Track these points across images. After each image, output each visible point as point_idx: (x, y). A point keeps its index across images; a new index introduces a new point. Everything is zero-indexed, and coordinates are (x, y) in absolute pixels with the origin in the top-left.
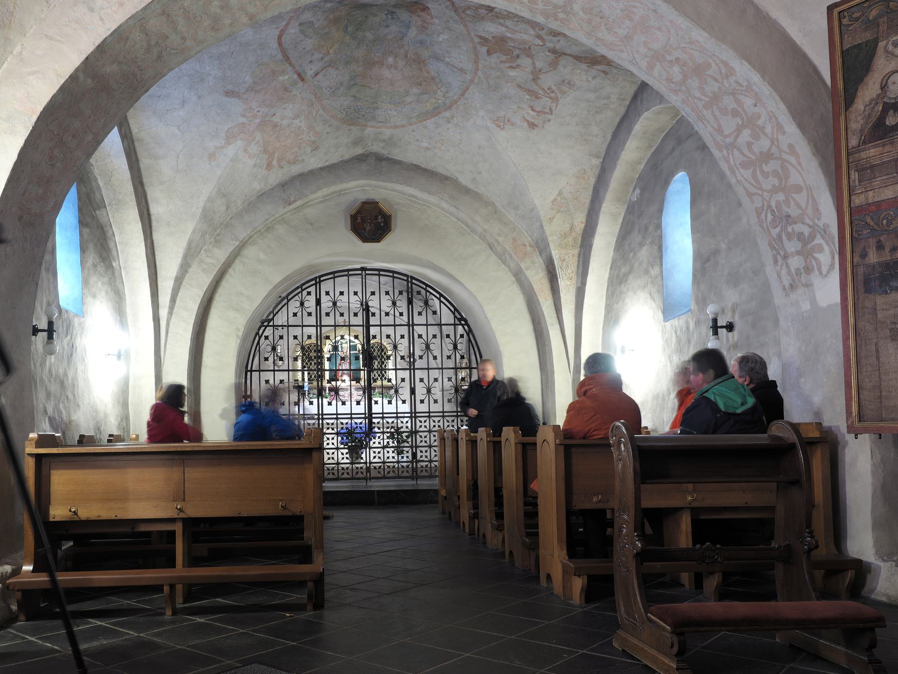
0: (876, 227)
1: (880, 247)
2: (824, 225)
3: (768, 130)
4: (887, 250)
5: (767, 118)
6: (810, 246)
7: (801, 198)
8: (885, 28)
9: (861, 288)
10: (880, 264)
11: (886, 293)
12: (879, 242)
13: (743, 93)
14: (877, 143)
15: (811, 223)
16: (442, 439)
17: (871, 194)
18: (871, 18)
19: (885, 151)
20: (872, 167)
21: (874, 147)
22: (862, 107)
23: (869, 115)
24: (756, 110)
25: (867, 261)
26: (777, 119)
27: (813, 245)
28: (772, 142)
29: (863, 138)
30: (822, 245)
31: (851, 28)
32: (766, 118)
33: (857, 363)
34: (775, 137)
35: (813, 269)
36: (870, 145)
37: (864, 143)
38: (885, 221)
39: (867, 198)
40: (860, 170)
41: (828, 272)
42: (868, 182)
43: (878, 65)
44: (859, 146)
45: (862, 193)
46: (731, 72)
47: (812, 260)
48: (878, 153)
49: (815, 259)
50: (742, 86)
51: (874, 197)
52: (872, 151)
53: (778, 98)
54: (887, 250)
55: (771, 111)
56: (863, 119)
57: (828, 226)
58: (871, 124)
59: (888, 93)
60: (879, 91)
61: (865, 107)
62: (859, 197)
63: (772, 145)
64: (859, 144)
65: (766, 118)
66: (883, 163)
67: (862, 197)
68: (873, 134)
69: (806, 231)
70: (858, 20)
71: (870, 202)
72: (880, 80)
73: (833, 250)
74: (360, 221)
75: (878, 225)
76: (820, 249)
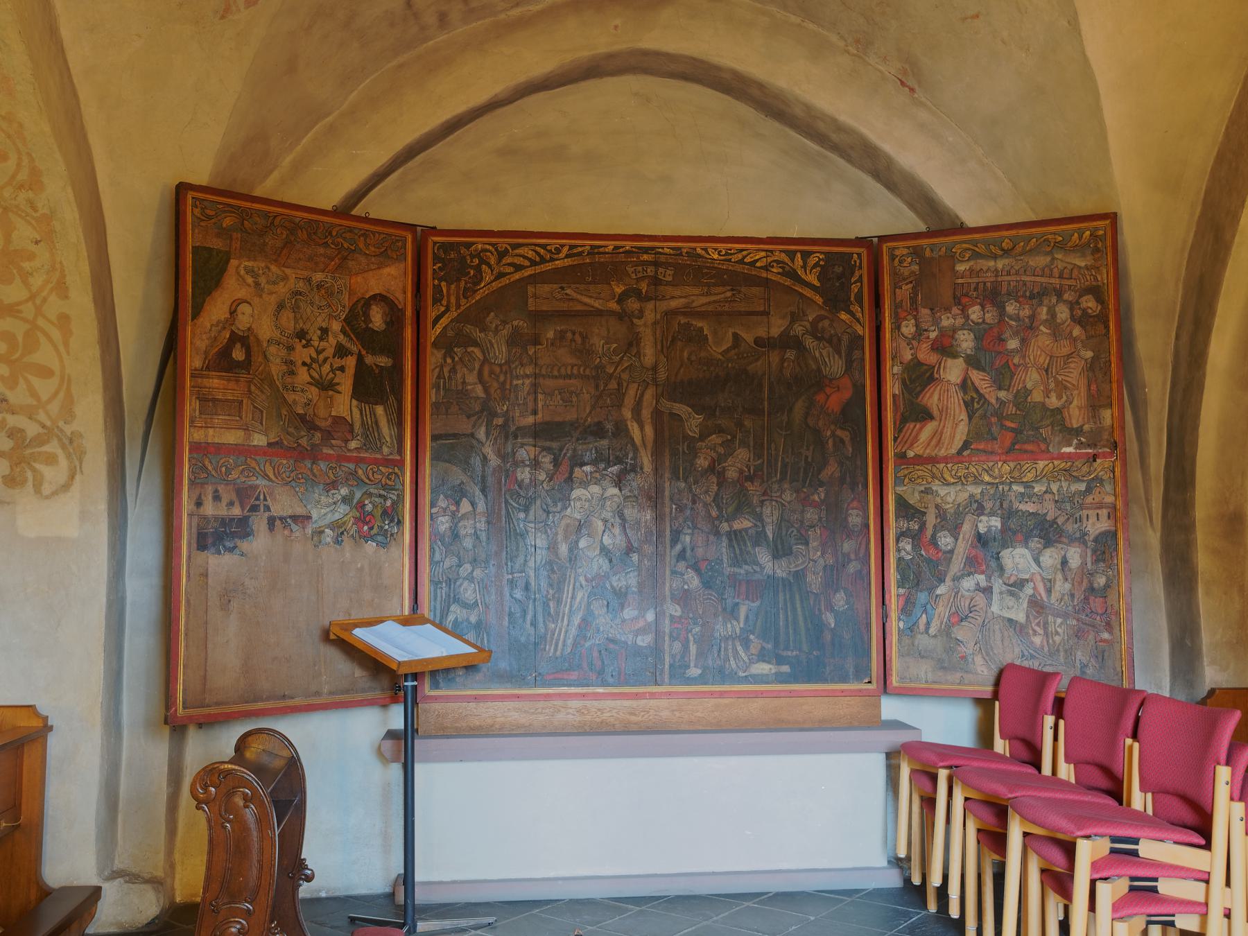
0: (213, 472)
1: (217, 498)
2: (72, 433)
3: (37, 281)
4: (225, 501)
5: (46, 267)
6: (31, 451)
7: (45, 387)
8: (238, 246)
9: (194, 545)
10: (216, 518)
11: (219, 553)
12: (216, 491)
13: (28, 218)
14: (221, 374)
15: (48, 423)
16: (1121, 919)
17: (211, 431)
18: (224, 225)
19: (230, 388)
20: (214, 400)
21: (220, 377)
22: (209, 326)
23: (215, 338)
24: (32, 247)
25: (201, 511)
26: (63, 276)
27: (40, 453)
28: (32, 297)
29: (207, 362)
30: (57, 456)
31: (202, 224)
32: (43, 266)
33: (186, 635)
34: (44, 294)
35: (25, 481)
36: (214, 373)
37: (208, 368)
38: (224, 469)
39: (206, 436)
40: (203, 399)
41: (55, 493)
42: (209, 416)
43: (228, 284)
44: (202, 370)
45: (202, 427)
46: (35, 181)
47: (26, 469)
48: (221, 387)
49: (34, 470)
50: (36, 211)
51: (214, 436)
52: (216, 381)
53: (86, 254)
54: (225, 501)
55: (61, 263)
56: (207, 339)
57: (81, 436)
58: (217, 349)
59: (236, 322)
60: (228, 315)
61: (212, 325)
62: (198, 431)
63: (27, 301)
64: (203, 367)
65: (43, 266)
66: (227, 401)
67: (202, 432)
68: (217, 361)
69: (32, 430)
70: (211, 219)
71: (209, 441)
72: (229, 303)
73: (75, 467)
74: (499, 462)
75: (216, 472)
76: (51, 460)
